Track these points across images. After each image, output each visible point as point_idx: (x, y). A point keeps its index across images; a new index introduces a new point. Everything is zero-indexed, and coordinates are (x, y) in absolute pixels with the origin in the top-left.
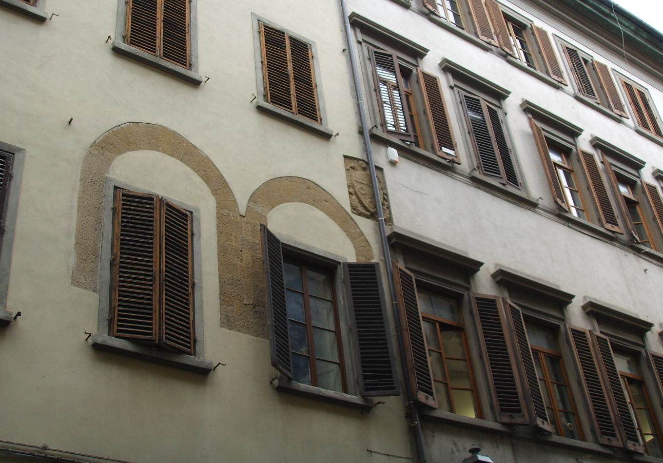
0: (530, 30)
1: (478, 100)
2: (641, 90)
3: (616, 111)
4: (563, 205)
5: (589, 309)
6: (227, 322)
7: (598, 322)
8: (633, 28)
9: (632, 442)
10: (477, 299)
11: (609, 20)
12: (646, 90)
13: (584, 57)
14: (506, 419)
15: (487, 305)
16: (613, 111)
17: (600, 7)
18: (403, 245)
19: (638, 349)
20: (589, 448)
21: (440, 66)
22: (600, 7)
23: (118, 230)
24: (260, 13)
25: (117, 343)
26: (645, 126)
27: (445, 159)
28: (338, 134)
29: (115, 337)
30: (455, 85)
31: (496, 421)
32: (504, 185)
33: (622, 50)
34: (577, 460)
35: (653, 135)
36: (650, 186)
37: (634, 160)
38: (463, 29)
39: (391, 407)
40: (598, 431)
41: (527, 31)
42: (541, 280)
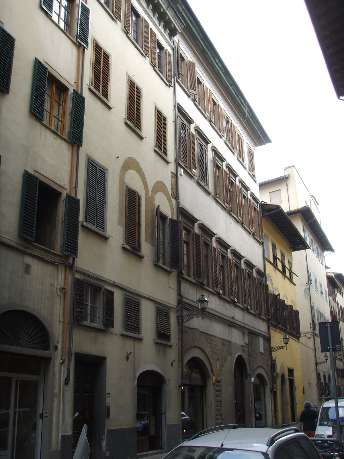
0: (217, 106)
1: (203, 146)
2: (214, 99)
3: (234, 149)
4: (268, 245)
5: (246, 261)
6: (146, 241)
7: (234, 256)
8: (248, 111)
9: (216, 288)
10: (196, 234)
11: (242, 106)
12: (203, 82)
13: (198, 77)
14: (197, 280)
15: (198, 236)
16: (205, 113)
17: (242, 100)
18: (183, 212)
19: (191, 229)
20: (226, 299)
21: (212, 148)
22: (242, 100)
23: (127, 204)
24: (131, 75)
25: (128, 247)
26: (240, 157)
27: (193, 174)
28: (146, 137)
29: (127, 244)
30: (198, 138)
31: (194, 279)
32: (205, 185)
33: (244, 123)
34: (208, 295)
35: (241, 160)
36: (193, 134)
37: (183, 111)
38: (200, 106)
39: (174, 273)
40: (266, 314)
41: (216, 106)
42: (208, 226)
